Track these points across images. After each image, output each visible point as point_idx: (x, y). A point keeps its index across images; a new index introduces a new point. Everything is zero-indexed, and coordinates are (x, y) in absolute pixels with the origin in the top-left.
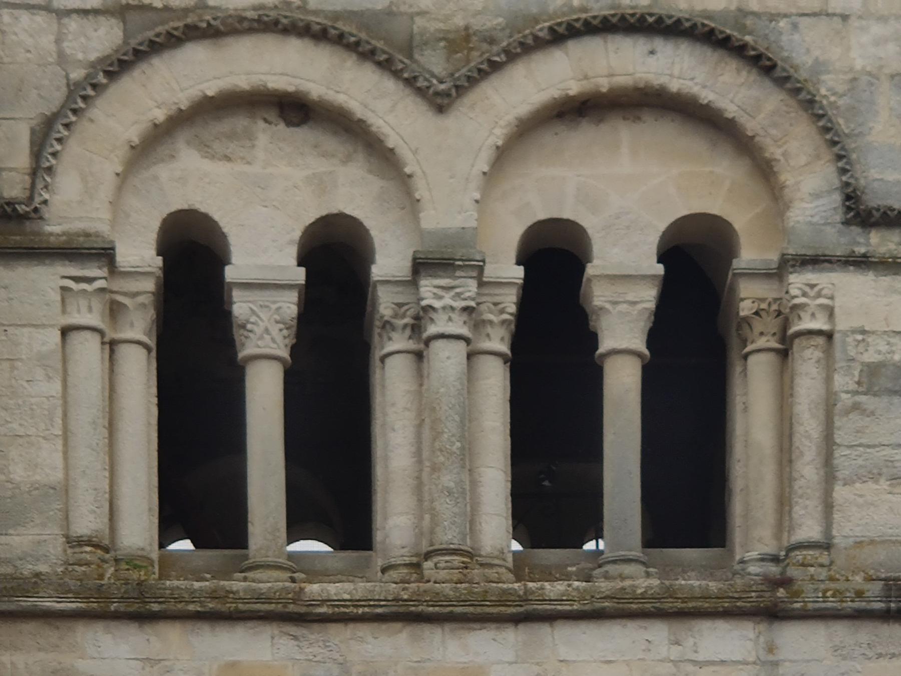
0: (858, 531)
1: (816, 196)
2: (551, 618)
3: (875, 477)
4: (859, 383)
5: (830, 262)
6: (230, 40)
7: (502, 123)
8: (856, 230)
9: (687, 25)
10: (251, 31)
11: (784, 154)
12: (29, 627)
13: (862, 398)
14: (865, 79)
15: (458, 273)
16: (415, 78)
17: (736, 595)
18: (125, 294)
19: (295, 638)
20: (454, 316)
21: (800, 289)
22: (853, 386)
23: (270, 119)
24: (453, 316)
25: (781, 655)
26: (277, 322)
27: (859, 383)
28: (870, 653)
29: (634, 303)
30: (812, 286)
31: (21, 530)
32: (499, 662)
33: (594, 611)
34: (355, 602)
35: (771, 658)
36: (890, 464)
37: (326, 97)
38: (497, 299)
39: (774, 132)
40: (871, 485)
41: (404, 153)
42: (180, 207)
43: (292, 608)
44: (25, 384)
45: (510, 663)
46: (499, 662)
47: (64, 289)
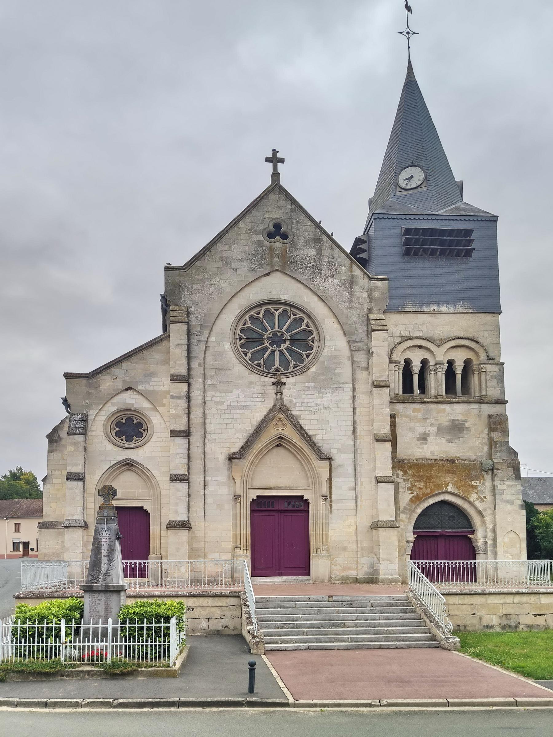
1: (484, 356)
2: (453, 403)
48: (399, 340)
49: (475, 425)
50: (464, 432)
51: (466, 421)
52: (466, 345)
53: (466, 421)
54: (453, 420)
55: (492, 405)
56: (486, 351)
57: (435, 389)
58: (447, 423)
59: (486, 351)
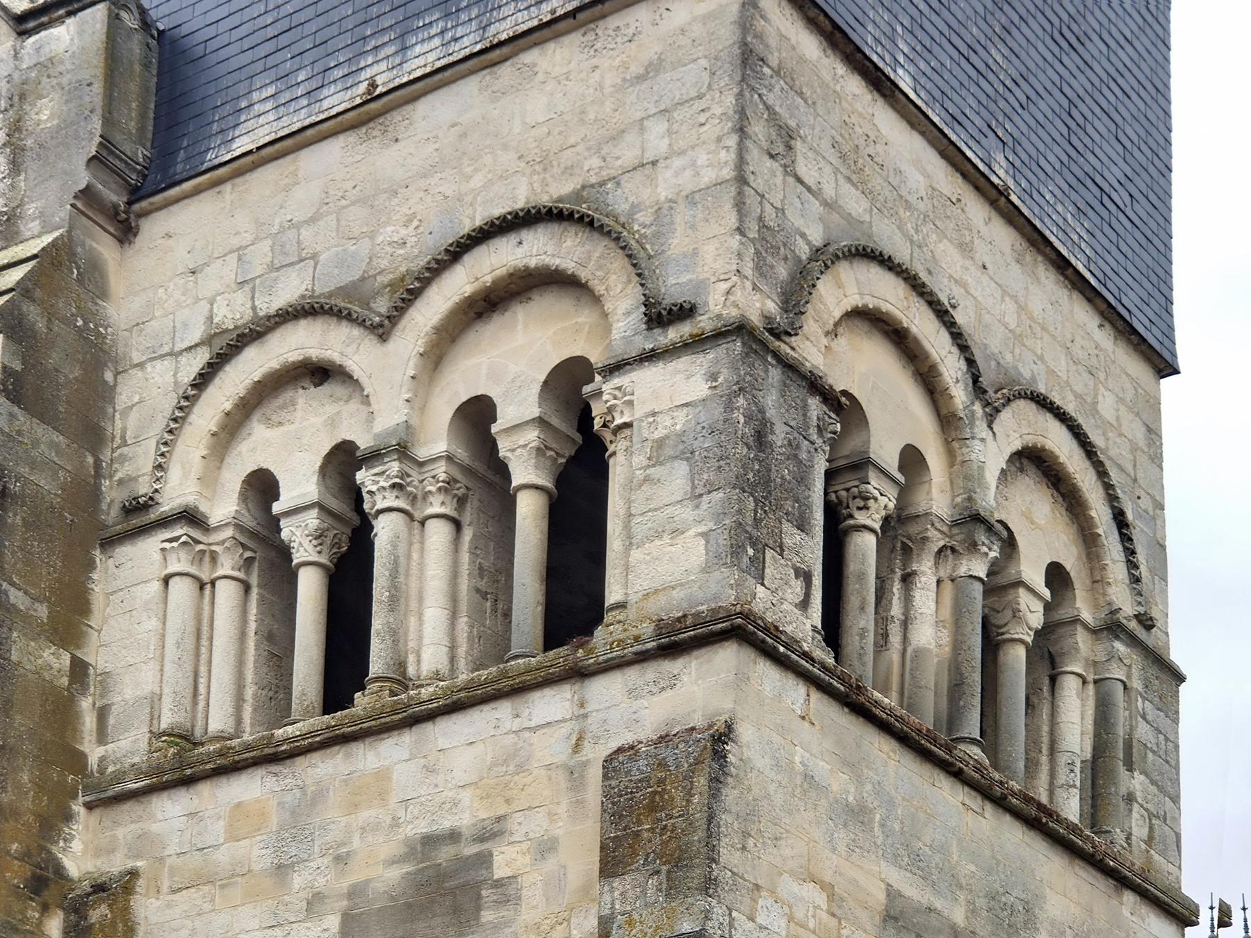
0: (646, 585)
1: (628, 314)
2: (430, 716)
3: (659, 535)
4: (649, 459)
5: (629, 364)
6: (269, 336)
7: (422, 335)
8: (657, 331)
9: (533, 211)
10: (277, 325)
11: (606, 289)
12: (127, 806)
13: (652, 470)
14: (666, 206)
15: (386, 460)
16: (364, 321)
17: (549, 664)
18: (217, 544)
19: (276, 774)
20: (387, 494)
21: (609, 394)
22: (646, 462)
23: (306, 385)
24: (386, 494)
25: (589, 707)
26: (308, 536)
27: (649, 459)
28: (655, 690)
29: (525, 446)
30: (619, 388)
31: (127, 735)
32: (400, 762)
33: (454, 703)
34: (303, 736)
35: (582, 711)
36: (671, 520)
37: (322, 356)
38: (433, 473)
39: (598, 273)
40: (658, 542)
41: (364, 381)
42: (252, 469)
43: (267, 751)
44: (136, 626)
45: (406, 761)
46: (400, 762)
47: (163, 550)
48: (200, 359)
49: (545, 848)
50: (487, 916)
51: (491, 832)
52: (533, 263)
53: (491, 832)
54: (430, 841)
55: (651, 671)
56: (639, 266)
57: (766, 630)
58: (394, 874)
59: (639, 266)
